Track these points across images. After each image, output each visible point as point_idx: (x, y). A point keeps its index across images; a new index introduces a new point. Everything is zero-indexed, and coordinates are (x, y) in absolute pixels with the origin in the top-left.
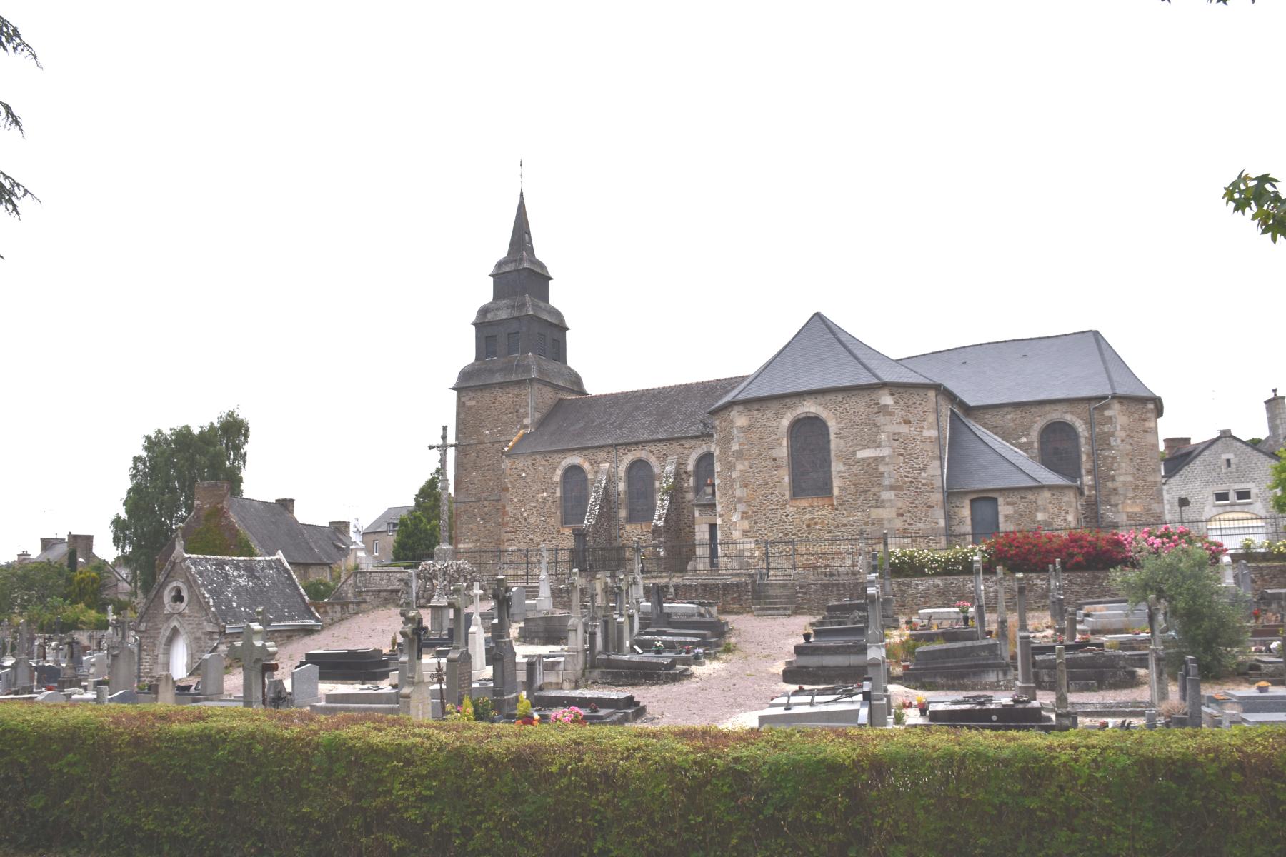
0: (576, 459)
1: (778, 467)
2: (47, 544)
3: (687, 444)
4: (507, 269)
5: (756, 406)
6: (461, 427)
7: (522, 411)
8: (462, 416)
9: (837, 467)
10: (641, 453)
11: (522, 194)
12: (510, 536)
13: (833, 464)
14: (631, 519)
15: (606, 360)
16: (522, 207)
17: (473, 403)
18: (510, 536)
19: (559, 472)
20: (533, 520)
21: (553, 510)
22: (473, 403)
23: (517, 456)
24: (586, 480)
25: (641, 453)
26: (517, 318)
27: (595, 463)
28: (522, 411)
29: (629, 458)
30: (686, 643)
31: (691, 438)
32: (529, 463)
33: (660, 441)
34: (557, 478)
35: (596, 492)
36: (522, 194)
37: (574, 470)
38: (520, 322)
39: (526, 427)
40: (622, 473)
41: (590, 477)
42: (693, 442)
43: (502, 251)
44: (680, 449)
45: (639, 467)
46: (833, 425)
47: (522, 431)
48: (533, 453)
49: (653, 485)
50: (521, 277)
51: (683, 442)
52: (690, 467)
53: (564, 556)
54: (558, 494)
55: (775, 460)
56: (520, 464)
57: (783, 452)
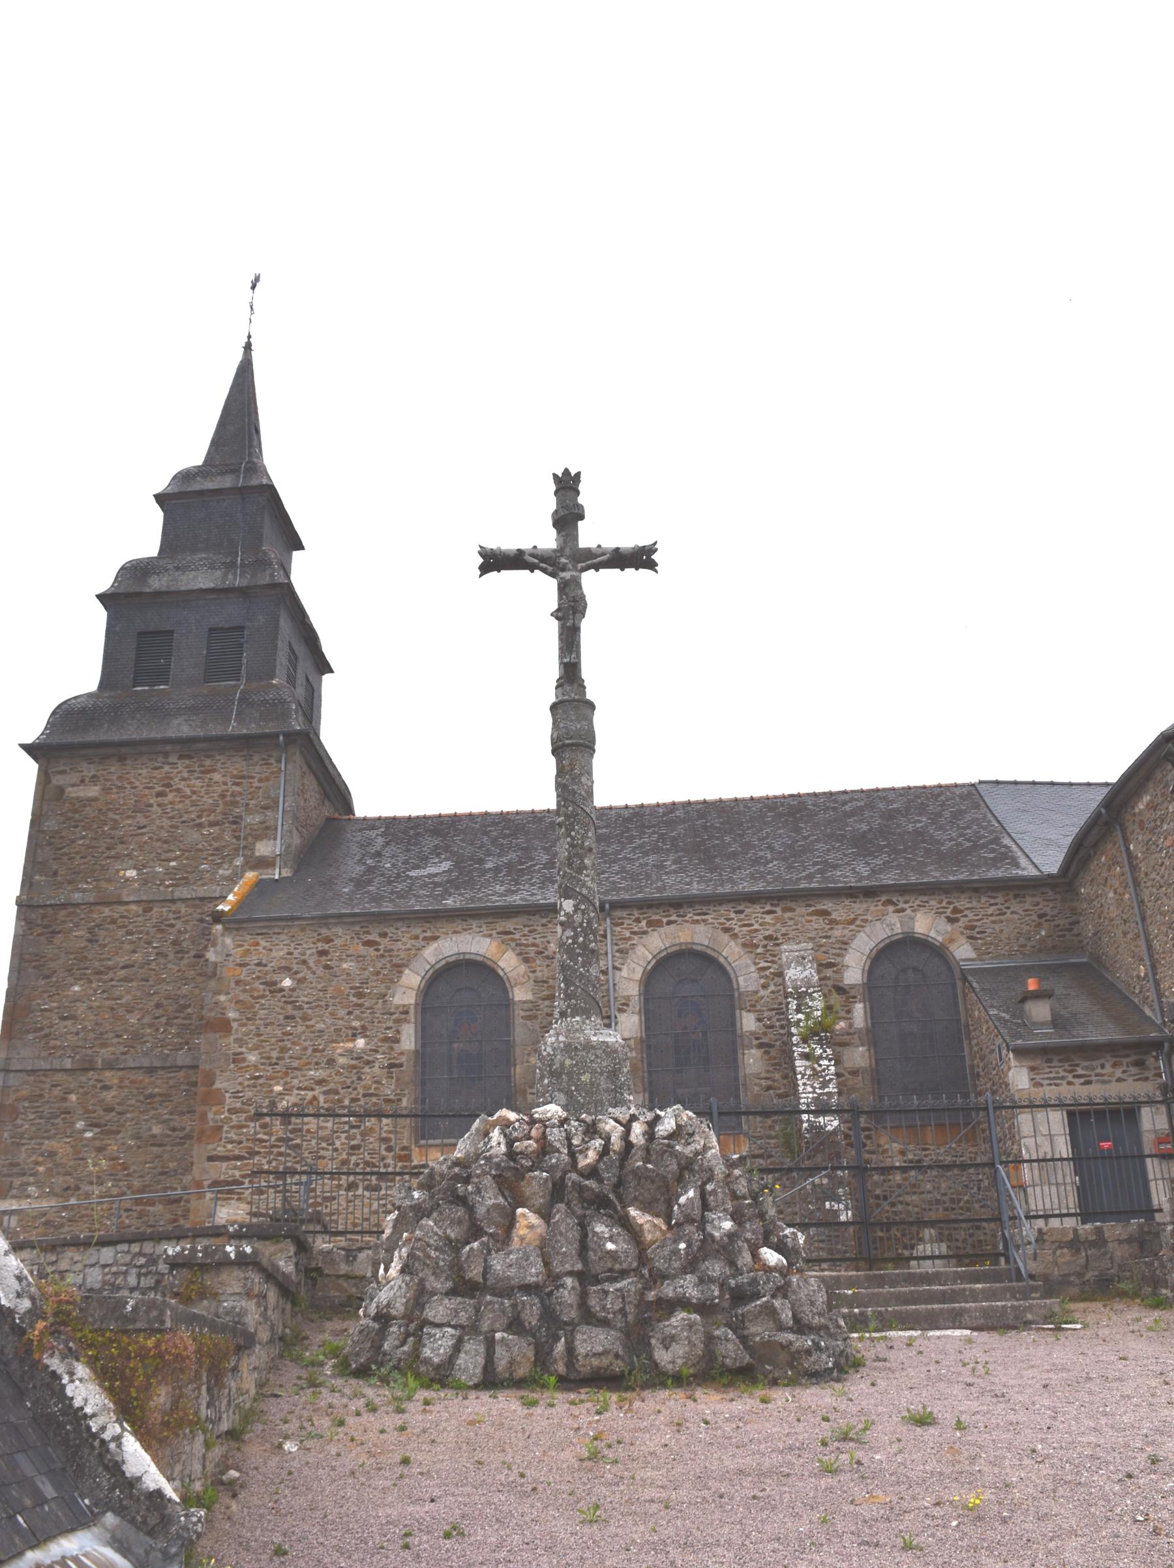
0: (477, 944)
3: (840, 910)
4: (196, 487)
7: (252, 819)
8: (50, 824)
10: (694, 933)
11: (248, 347)
12: (223, 1170)
15: (423, 719)
16: (245, 373)
17: (93, 791)
18: (223, 1170)
19: (412, 979)
22: (93, 791)
23: (269, 925)
24: (507, 1004)
25: (694, 933)
26: (243, 592)
29: (654, 943)
31: (851, 893)
32: (309, 947)
33: (752, 898)
36: (248, 347)
39: (263, 863)
42: (859, 907)
44: (819, 923)
47: (251, 875)
48: (325, 920)
49: (732, 1023)
50: (228, 509)
51: (827, 905)
52: (853, 975)
54: (408, 1040)
56: (276, 949)
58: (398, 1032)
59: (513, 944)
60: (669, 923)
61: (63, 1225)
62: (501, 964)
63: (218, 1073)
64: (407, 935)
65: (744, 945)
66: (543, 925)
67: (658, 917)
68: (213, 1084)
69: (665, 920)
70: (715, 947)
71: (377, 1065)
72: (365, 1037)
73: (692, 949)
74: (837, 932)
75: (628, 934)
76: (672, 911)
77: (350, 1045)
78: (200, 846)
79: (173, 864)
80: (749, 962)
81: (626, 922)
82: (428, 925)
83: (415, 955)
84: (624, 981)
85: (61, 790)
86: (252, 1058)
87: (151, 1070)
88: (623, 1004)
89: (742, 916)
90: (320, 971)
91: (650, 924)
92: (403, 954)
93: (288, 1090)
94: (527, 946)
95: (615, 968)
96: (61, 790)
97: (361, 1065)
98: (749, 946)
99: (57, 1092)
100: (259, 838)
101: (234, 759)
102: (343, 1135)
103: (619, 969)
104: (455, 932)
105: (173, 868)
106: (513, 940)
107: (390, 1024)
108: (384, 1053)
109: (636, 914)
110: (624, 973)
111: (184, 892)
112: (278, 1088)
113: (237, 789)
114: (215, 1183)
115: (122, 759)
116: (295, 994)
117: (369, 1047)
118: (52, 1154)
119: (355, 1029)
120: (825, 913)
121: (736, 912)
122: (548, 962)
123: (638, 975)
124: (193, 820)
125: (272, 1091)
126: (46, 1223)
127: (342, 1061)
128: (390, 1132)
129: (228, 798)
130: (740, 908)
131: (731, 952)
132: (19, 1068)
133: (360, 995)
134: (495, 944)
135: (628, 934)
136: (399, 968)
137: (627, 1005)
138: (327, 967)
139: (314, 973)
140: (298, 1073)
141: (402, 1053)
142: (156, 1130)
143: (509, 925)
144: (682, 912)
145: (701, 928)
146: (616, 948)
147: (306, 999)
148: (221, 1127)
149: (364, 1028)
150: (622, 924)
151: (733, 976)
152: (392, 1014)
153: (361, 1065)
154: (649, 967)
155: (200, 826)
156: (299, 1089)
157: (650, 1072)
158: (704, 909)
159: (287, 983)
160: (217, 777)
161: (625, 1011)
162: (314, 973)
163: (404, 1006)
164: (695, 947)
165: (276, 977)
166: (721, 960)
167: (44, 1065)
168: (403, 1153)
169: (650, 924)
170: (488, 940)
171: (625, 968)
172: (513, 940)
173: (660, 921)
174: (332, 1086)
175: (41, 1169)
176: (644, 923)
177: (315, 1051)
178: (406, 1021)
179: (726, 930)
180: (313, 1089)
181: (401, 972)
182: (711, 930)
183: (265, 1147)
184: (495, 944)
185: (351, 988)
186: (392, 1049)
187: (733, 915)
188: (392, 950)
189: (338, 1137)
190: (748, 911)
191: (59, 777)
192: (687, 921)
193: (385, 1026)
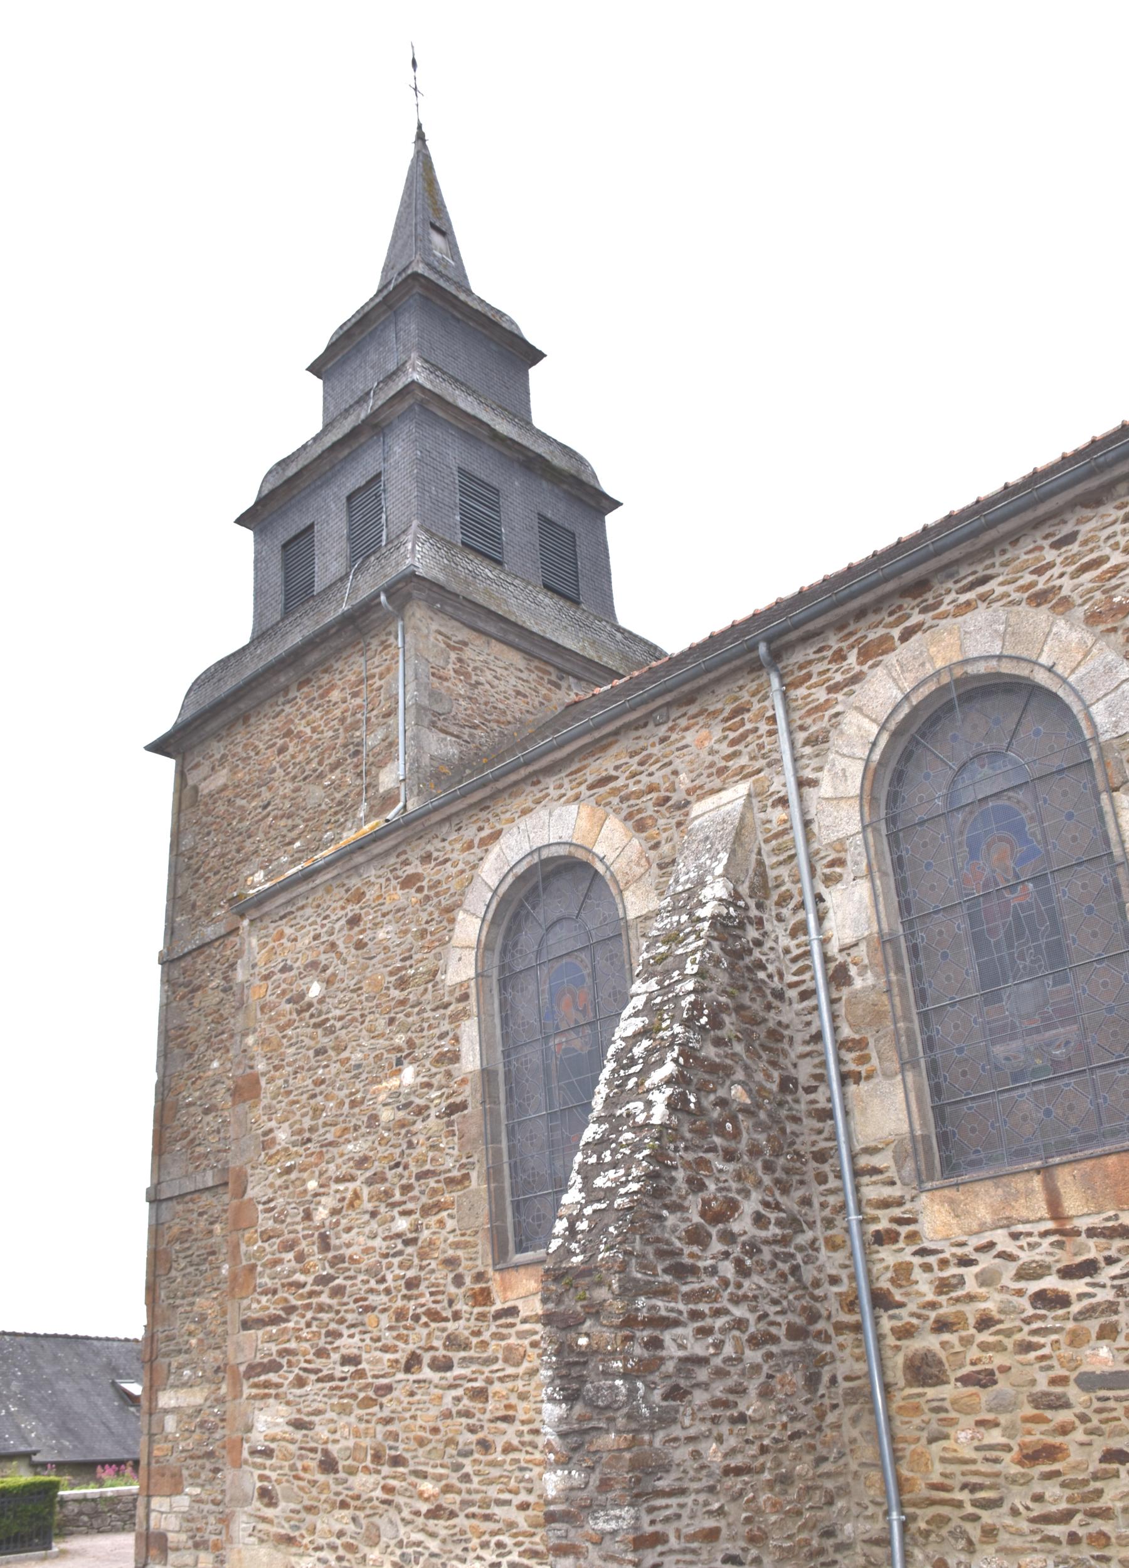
6: (184, 882)
7: (373, 740)
11: (421, 137)
14: (952, 1149)
20: (360, 1240)
24: (617, 932)
27: (656, 814)
28: (373, 740)
30: (491, 764)
34: (460, 969)
35: (659, 967)
36: (421, 137)
39: (389, 799)
41: (636, 903)
53: (895, 1247)
54: (471, 1061)
58: (457, 1039)
59: (615, 801)
60: (905, 636)
61: (216, 1427)
62: (599, 850)
63: (250, 1172)
64: (458, 846)
65: (1093, 619)
66: (663, 740)
67: (881, 631)
68: (244, 1192)
69: (896, 633)
70: (1019, 651)
71: (433, 1112)
72: (415, 1060)
73: (967, 679)
75: (821, 695)
76: (908, 603)
77: (394, 1082)
78: (323, 807)
79: (298, 844)
80: (1111, 657)
81: (816, 668)
82: (484, 815)
83: (471, 880)
84: (828, 808)
88: (832, 864)
89: (1075, 548)
90: (351, 956)
91: (865, 654)
92: (454, 885)
94: (639, 794)
95: (801, 783)
97: (411, 1118)
101: (351, 660)
102: (396, 1261)
103: (813, 783)
104: (525, 812)
105: (299, 851)
106: (614, 792)
107: (445, 1026)
108: (440, 1088)
109: (834, 642)
110: (826, 789)
112: (312, 1185)
113: (358, 701)
116: (324, 1008)
117: (420, 1080)
119: (399, 1049)
121: (1056, 545)
122: (678, 816)
123: (853, 786)
124: (315, 770)
125: (305, 1191)
126: (202, 1425)
127: (386, 1115)
128: (456, 1246)
129: (349, 720)
130: (1066, 530)
132: (168, 1195)
133: (402, 984)
134: (585, 811)
135: (821, 695)
136: (449, 912)
137: (840, 862)
138: (360, 945)
139: (345, 962)
140: (334, 1151)
141: (464, 1081)
144: (930, 597)
145: (980, 616)
146: (801, 736)
147: (338, 1013)
148: (254, 1266)
149: (411, 1043)
150: (809, 676)
151: (1076, 708)
152: (446, 1006)
153: (411, 1118)
154: (876, 756)
155: (321, 776)
156: (338, 1180)
157: (924, 1017)
158: (981, 570)
161: (838, 879)
162: (345, 962)
163: (461, 984)
164: (972, 669)
165: (301, 985)
166: (1041, 677)
168: (477, 1286)
169: (865, 654)
170: (574, 807)
171: (825, 777)
172: (614, 792)
173: (887, 638)
174: (377, 1167)
175: (194, 1341)
176: (852, 657)
177: (353, 1104)
178: (465, 1013)
179: (1039, 599)
180: (353, 1179)
181: (452, 921)
182: (1001, 613)
183: (302, 1297)
184: (585, 811)
185: (391, 974)
186: (449, 1074)
187: (1050, 555)
188: (439, 882)
189: (389, 1267)
190: (1085, 529)
191: (194, 772)
192: (945, 615)
193: (437, 1032)
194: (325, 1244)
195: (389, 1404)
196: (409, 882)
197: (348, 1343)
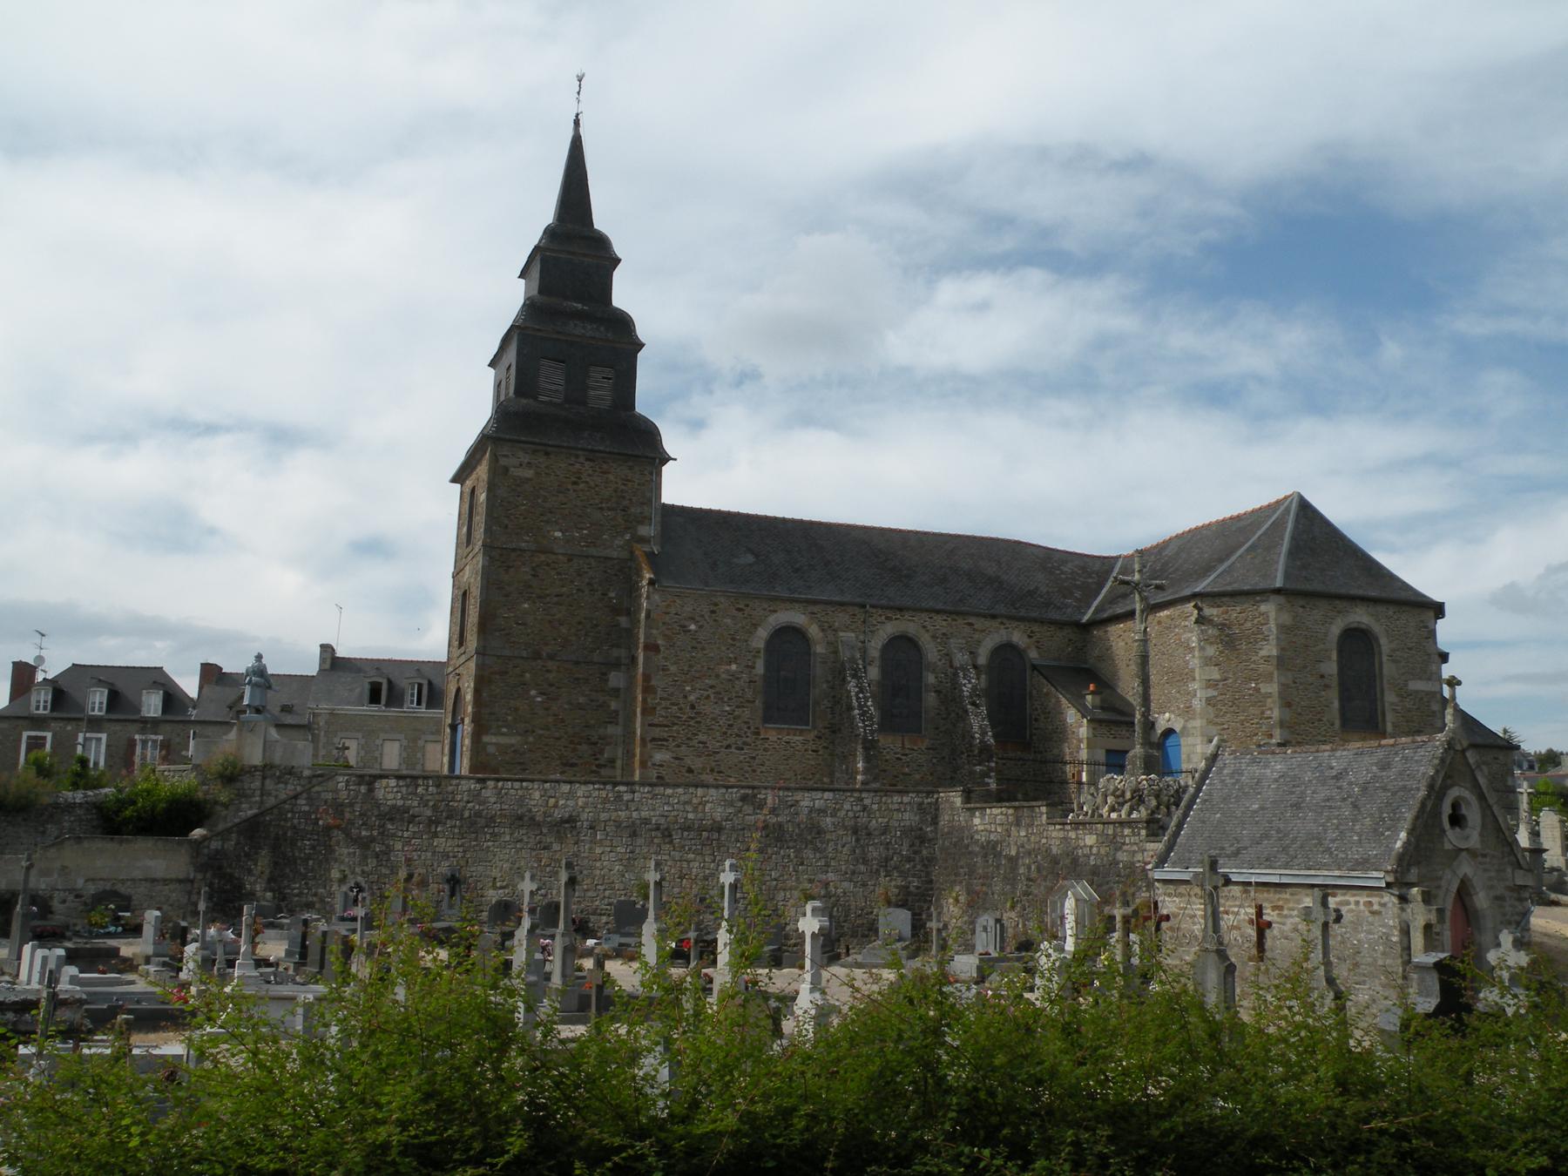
0: (797, 617)
1: (1327, 686)
2: (1453, 682)
3: (979, 624)
5: (1302, 602)
9: (1390, 697)
11: (577, 123)
13: (1386, 693)
17: (529, 473)
19: (763, 634)
21: (749, 695)
22: (529, 473)
29: (889, 629)
36: (577, 123)
37: (788, 636)
38: (572, 347)
40: (875, 653)
42: (988, 623)
43: (544, 211)
44: (967, 629)
45: (903, 646)
46: (1385, 644)
50: (572, 265)
51: (972, 620)
54: (760, 668)
55: (1322, 676)
57: (1331, 667)
74: (976, 636)
85: (506, 469)
86: (673, 669)
87: (577, 663)
93: (694, 690)
96: (506, 469)
98: (934, 637)
99: (517, 671)
100: (641, 523)
111: (593, 551)
114: (654, 739)
115: (547, 454)
118: (516, 709)
120: (970, 624)
131: (925, 640)
136: (755, 626)
142: (581, 700)
143: (815, 609)
159: (693, 627)
160: (611, 477)
167: (507, 653)
194: (693, 707)
195: (718, 757)
196: (739, 610)
197: (701, 737)
